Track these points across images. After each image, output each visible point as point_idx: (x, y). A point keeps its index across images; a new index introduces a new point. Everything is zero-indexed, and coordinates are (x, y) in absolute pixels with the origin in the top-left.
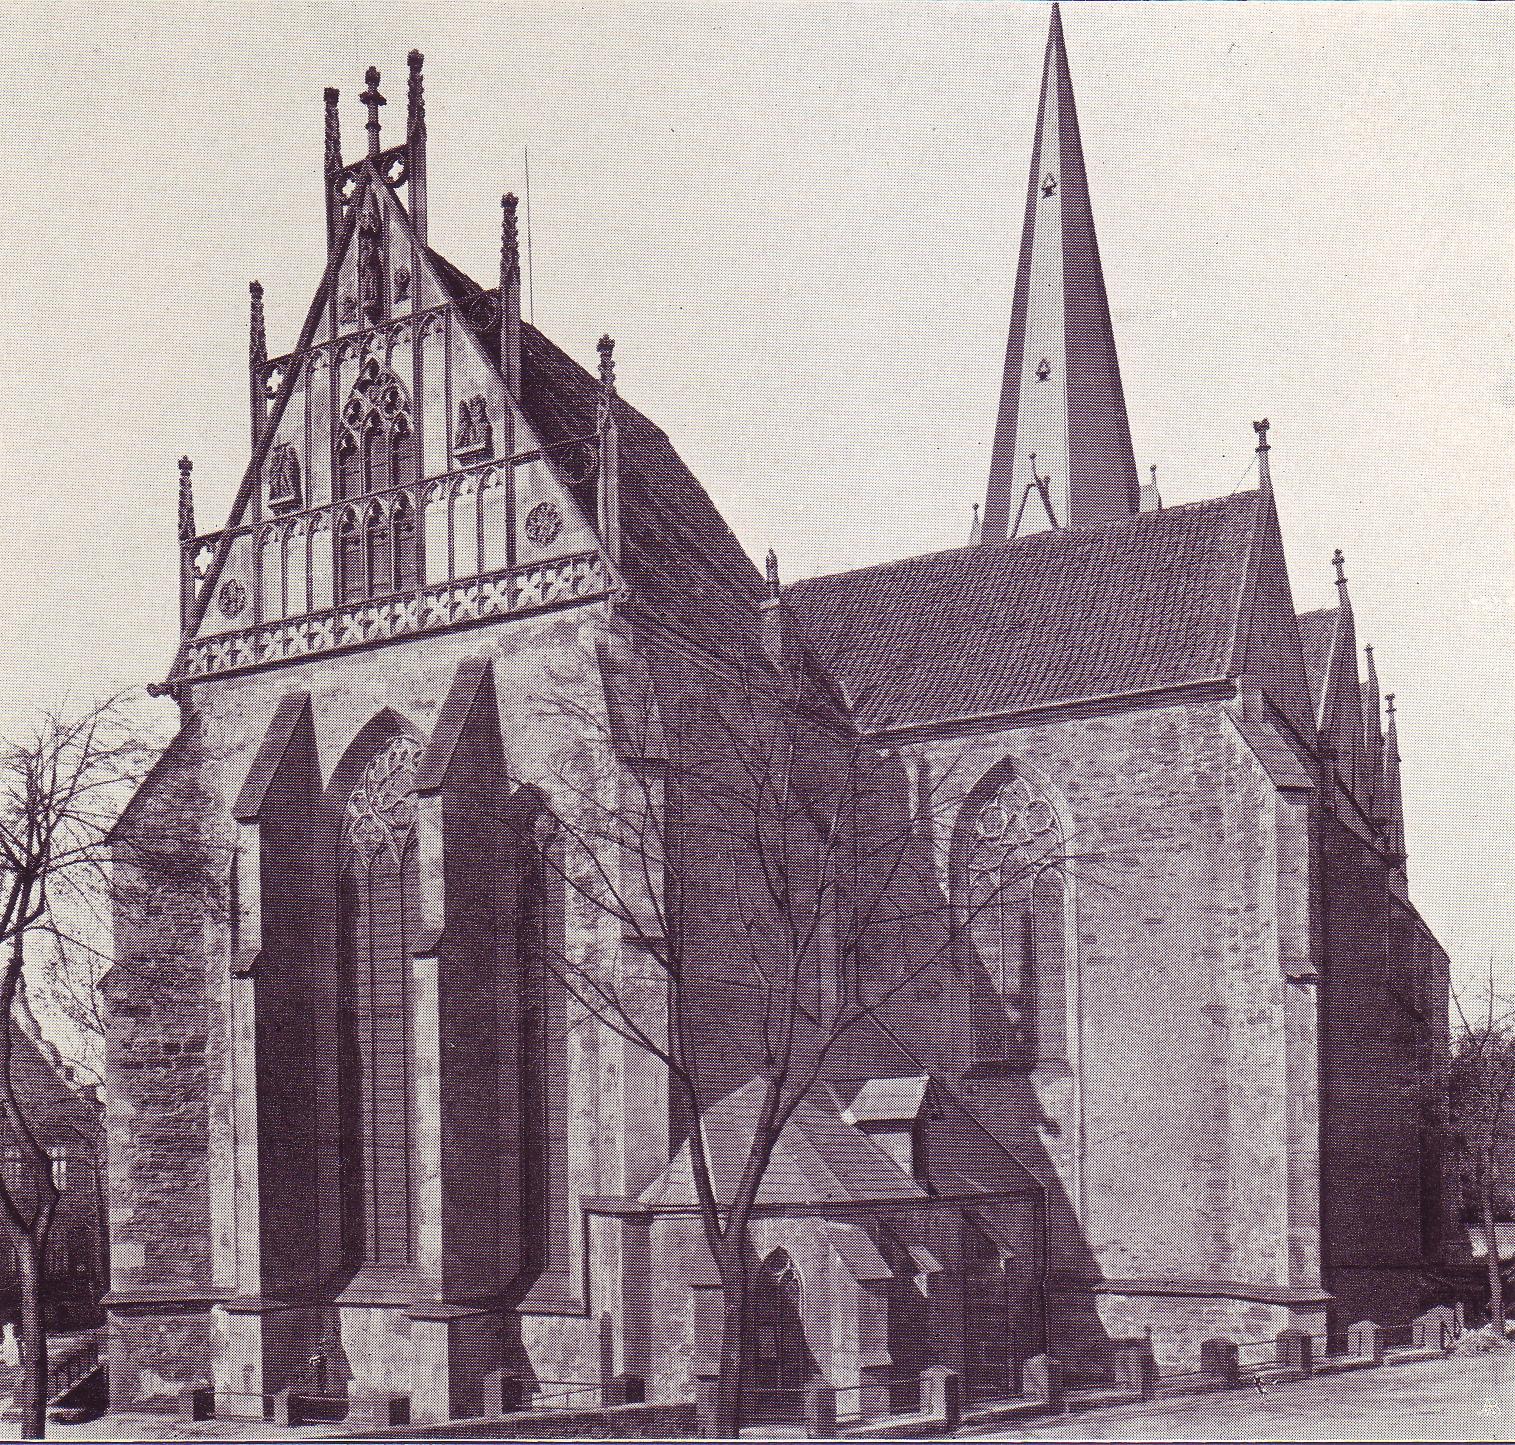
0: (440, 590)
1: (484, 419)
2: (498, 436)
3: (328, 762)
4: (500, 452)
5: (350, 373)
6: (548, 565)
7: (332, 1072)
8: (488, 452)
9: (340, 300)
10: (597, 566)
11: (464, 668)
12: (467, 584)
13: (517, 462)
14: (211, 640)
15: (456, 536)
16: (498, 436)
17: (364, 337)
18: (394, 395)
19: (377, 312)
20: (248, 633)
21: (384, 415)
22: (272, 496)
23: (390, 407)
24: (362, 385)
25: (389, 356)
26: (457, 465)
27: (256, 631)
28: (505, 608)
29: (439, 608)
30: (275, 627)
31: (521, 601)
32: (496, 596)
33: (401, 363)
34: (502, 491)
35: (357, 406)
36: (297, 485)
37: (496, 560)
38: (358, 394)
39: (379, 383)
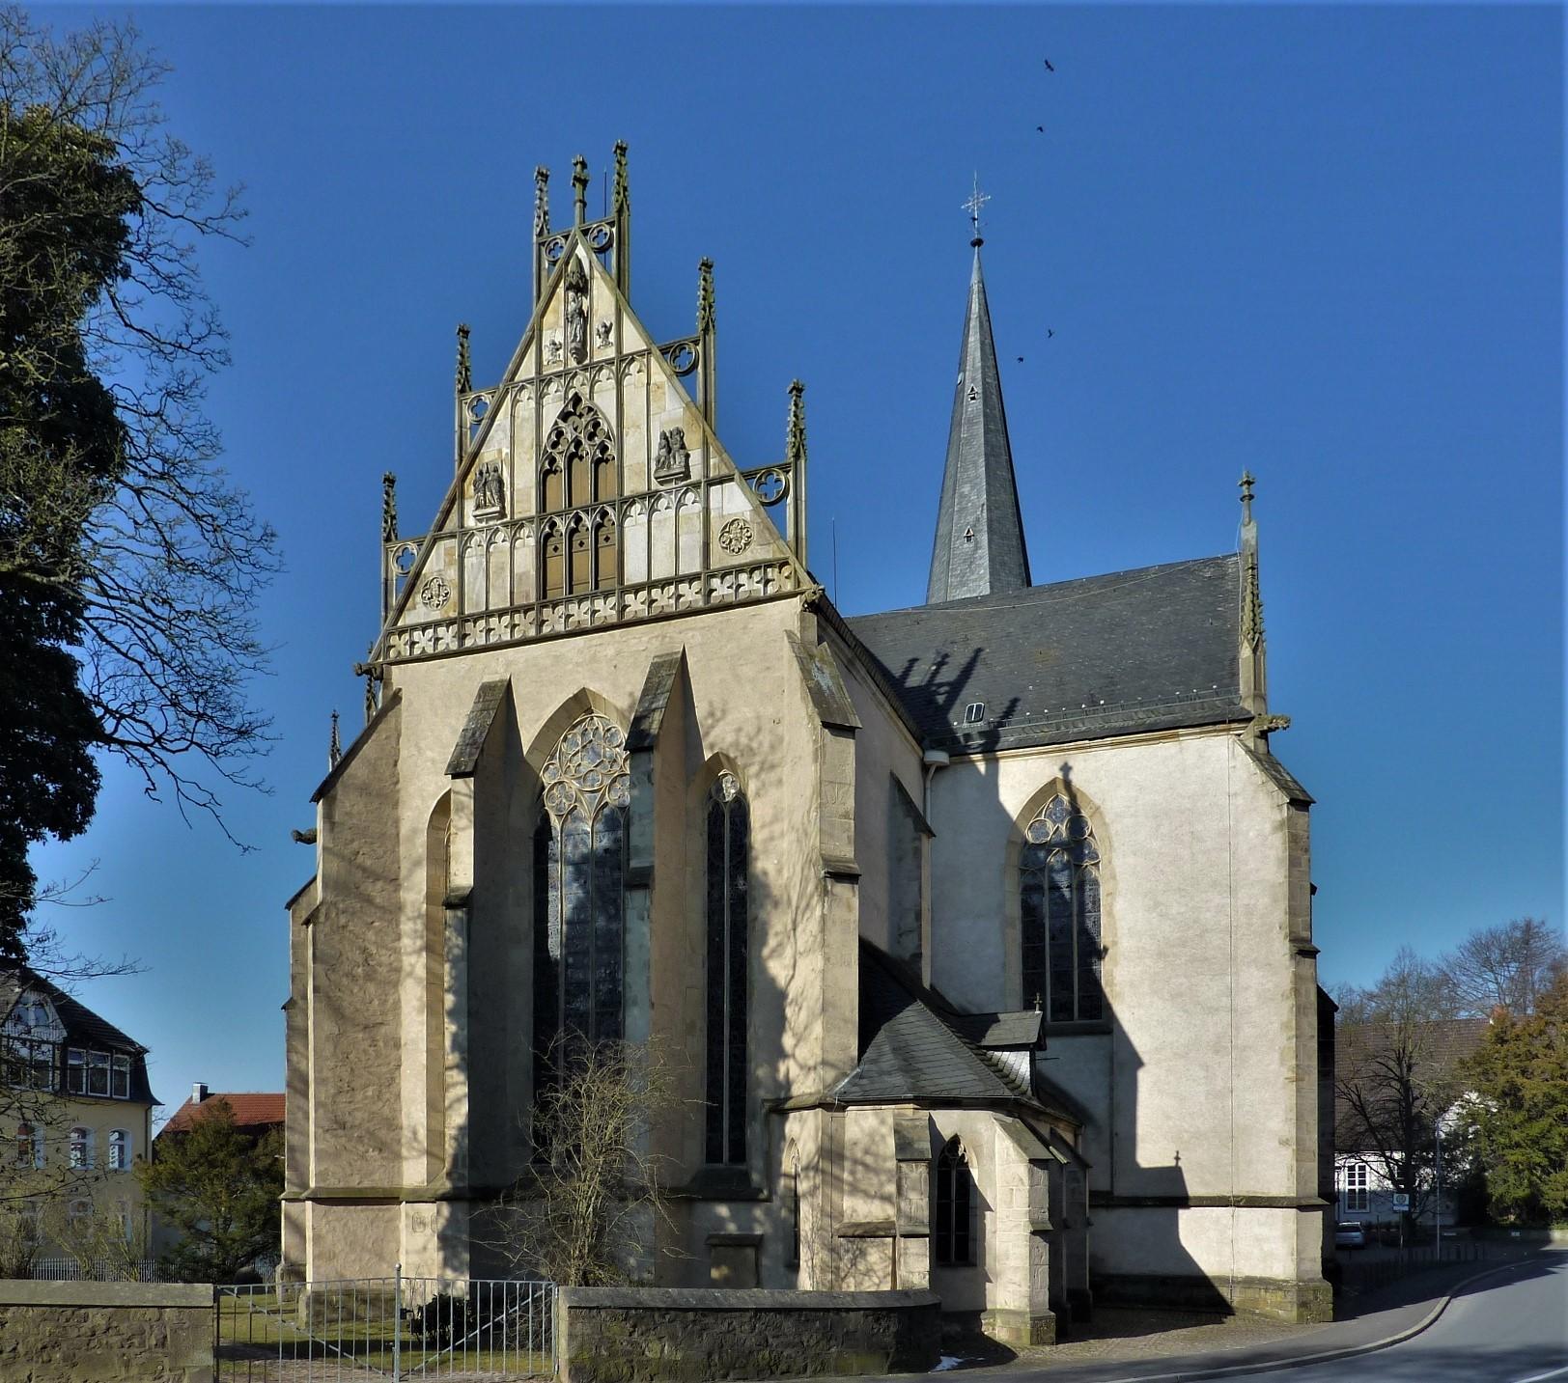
0: (636, 589)
1: (683, 447)
2: (696, 457)
3: (527, 737)
4: (696, 474)
5: (553, 408)
6: (739, 570)
7: (1248, 615)
8: (687, 475)
9: (546, 342)
10: (786, 571)
11: (486, 689)
12: (664, 584)
13: (710, 483)
14: (413, 628)
15: (653, 543)
16: (696, 457)
17: (567, 375)
18: (597, 425)
19: (581, 353)
20: (450, 622)
21: (586, 444)
22: (478, 507)
23: (591, 436)
24: (565, 416)
25: (591, 392)
26: (655, 485)
27: (462, 620)
28: (430, 650)
29: (636, 605)
30: (476, 618)
31: (441, 647)
32: (691, 594)
33: (604, 400)
34: (699, 507)
35: (560, 434)
36: (502, 499)
37: (692, 564)
38: (561, 424)
39: (581, 416)
